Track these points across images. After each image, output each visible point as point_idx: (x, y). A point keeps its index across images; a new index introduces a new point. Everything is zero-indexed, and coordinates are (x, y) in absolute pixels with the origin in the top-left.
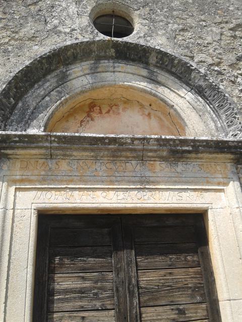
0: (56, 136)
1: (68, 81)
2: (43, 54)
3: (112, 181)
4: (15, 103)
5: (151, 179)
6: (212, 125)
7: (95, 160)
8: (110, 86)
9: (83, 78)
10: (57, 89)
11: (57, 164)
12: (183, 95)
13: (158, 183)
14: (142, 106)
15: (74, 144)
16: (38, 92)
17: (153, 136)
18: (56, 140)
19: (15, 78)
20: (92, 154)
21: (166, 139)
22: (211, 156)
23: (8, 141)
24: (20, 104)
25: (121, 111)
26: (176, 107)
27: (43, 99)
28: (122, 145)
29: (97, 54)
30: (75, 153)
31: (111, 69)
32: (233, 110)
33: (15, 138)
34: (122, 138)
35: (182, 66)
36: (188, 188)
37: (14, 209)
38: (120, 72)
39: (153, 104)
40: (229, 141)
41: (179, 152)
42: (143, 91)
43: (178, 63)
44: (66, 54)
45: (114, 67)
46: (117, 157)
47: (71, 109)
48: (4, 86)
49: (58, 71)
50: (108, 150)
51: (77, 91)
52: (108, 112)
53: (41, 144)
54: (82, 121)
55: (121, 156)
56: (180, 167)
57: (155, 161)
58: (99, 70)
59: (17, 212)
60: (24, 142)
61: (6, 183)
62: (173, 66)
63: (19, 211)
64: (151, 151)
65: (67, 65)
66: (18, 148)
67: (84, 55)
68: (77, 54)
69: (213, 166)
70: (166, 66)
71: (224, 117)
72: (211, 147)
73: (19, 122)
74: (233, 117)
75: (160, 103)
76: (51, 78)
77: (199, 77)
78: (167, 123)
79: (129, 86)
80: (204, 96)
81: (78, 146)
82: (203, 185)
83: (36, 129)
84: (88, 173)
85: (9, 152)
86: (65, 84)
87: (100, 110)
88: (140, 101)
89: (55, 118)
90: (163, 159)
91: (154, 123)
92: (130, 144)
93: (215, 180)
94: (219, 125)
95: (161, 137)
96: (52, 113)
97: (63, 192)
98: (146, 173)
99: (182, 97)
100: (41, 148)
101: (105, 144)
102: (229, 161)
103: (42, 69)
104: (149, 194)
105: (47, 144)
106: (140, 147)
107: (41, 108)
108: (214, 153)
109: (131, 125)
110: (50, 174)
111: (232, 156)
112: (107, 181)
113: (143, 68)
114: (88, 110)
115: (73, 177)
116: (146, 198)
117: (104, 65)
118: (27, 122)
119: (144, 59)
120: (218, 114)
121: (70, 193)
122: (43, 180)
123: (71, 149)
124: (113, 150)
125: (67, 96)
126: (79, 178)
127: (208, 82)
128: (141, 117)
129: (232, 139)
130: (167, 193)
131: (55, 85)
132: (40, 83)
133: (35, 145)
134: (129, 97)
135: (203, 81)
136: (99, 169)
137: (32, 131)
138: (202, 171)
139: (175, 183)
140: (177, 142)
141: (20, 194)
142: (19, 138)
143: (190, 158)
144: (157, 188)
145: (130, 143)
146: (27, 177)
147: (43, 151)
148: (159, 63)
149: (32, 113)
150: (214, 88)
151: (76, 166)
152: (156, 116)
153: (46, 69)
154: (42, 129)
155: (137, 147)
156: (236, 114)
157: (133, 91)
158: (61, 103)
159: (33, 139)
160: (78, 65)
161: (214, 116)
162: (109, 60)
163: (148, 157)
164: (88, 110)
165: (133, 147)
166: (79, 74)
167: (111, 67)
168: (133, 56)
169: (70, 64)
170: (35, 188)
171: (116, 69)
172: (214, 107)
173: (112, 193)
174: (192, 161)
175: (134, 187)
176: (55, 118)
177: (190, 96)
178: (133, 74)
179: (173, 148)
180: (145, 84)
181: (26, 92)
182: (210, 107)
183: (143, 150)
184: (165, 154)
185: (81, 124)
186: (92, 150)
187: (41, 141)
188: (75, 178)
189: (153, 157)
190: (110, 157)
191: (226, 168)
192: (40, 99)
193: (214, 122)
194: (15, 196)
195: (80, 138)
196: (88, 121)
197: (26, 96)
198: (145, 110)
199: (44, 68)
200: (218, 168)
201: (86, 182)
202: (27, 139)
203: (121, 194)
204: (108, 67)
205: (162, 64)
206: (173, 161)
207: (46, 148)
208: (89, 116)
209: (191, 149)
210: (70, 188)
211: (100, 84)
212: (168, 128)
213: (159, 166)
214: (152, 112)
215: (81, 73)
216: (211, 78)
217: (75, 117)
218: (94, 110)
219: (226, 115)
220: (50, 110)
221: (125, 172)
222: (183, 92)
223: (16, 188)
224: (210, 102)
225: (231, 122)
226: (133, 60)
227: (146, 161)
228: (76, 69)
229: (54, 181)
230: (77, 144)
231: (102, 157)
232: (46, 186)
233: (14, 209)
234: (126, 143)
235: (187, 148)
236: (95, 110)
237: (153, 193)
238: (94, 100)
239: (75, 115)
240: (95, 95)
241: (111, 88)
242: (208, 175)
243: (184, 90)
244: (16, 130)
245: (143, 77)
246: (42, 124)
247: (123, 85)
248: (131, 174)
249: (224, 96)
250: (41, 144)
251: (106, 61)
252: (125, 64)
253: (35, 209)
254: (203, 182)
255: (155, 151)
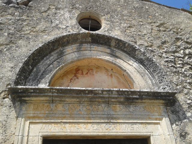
0: (56, 89)
1: (64, 56)
2: (50, 40)
3: (89, 117)
4: (32, 69)
5: (114, 116)
6: (150, 82)
7: (79, 104)
8: (88, 58)
9: (73, 54)
10: (57, 61)
11: (56, 107)
12: (131, 64)
13: (119, 119)
14: (107, 70)
15: (67, 94)
16: (46, 62)
17: (115, 89)
18: (56, 91)
19: (33, 54)
20: (78, 100)
21: (122, 91)
22: (150, 101)
23: (27, 92)
24: (35, 69)
25: (94, 73)
26: (127, 71)
27: (49, 66)
28: (96, 95)
29: (81, 41)
30: (67, 100)
31: (89, 49)
32: (162, 73)
33: (31, 90)
34: (96, 90)
35: (130, 47)
36: (137, 122)
37: (28, 136)
38: (94, 50)
39: (113, 69)
40: (161, 92)
41: (131, 99)
42: (107, 61)
43: (128, 46)
44: (63, 40)
45: (91, 48)
46: (93, 102)
47: (66, 71)
48: (26, 59)
49: (58, 50)
50: (87, 97)
51: (69, 61)
52: (87, 73)
53: (46, 94)
54: (71, 79)
55: (95, 101)
56: (132, 109)
57: (116, 104)
58: (82, 49)
59: (30, 138)
60: (36, 93)
61: (24, 119)
62: (125, 47)
63: (31, 137)
64: (114, 98)
65: (64, 46)
66: (33, 96)
67: (73, 41)
68: (70, 40)
69: (152, 108)
70: (121, 47)
71: (157, 77)
72: (150, 96)
73: (33, 80)
74: (162, 78)
75: (118, 69)
76: (54, 54)
77: (141, 54)
78: (122, 80)
79: (100, 58)
80: (144, 65)
81: (69, 95)
82: (146, 120)
83: (44, 85)
84: (75, 112)
85: (27, 99)
86: (62, 57)
87: (82, 72)
88: (106, 67)
89: (55, 78)
90: (121, 103)
91: (114, 80)
92: (101, 94)
93: (154, 117)
94: (154, 82)
95: (120, 89)
96: (54, 75)
97: (59, 125)
98: (111, 112)
99: (131, 65)
100: (46, 96)
101: (86, 94)
102: (162, 104)
103: (49, 49)
104: (113, 126)
105: (51, 94)
106: (107, 96)
107: (48, 72)
108: (152, 99)
109: (101, 82)
110: (51, 113)
111: (163, 102)
112: (87, 118)
113: (108, 48)
114: (75, 72)
115: (65, 115)
116: (111, 128)
117: (85, 46)
118: (38, 80)
119: (108, 43)
120: (153, 75)
121: (63, 125)
122: (47, 117)
123: (65, 97)
124: (90, 98)
125: (63, 65)
126: (69, 115)
127: (146, 56)
128: (106, 77)
129: (162, 91)
130: (124, 126)
131: (56, 58)
132: (48, 57)
133: (43, 94)
134: (99, 65)
135: (143, 56)
136: (81, 109)
137: (43, 85)
138: (145, 111)
139: (129, 118)
140: (130, 93)
141: (32, 126)
142: (34, 91)
143: (138, 103)
144: (118, 122)
145: (100, 93)
146: (37, 115)
147: (47, 98)
148: (117, 46)
149: (42, 74)
150: (150, 60)
151: (67, 108)
152: (115, 76)
153: (51, 49)
154: (48, 84)
155: (105, 96)
156: (164, 75)
157: (102, 61)
158: (60, 68)
159: (42, 91)
160: (70, 47)
161: (151, 76)
162: (87, 44)
163: (112, 102)
164: (75, 72)
165: (103, 96)
166: (70, 52)
167: (89, 48)
168: (101, 41)
169: (65, 46)
170: (42, 122)
171: (92, 49)
172: (150, 71)
173: (89, 125)
174: (139, 104)
175: (103, 121)
176: (55, 78)
177: (136, 65)
178: (102, 52)
179: (127, 96)
180: (109, 57)
181: (39, 62)
182: (148, 71)
183: (109, 98)
184: (122, 100)
185: (70, 81)
186: (78, 98)
187: (47, 92)
188: (67, 115)
189: (115, 102)
190: (89, 102)
191: (160, 108)
192: (47, 66)
193: (151, 80)
194: (29, 127)
195: (70, 90)
196: (75, 79)
197: (39, 65)
198: (109, 73)
199: (50, 49)
200: (155, 109)
201: (73, 118)
202: (38, 91)
203: (96, 126)
204: (87, 47)
205: (118, 46)
206: (127, 104)
207: (50, 96)
208: (75, 76)
209: (138, 97)
210: (63, 122)
211: (82, 57)
212: (123, 83)
213: (118, 107)
214: (113, 74)
215: (72, 51)
216: (148, 54)
217: (67, 76)
218: (78, 73)
219: (158, 76)
220: (53, 73)
221: (98, 111)
222: (131, 62)
223: (30, 122)
224: (148, 68)
225: (161, 80)
226: (102, 44)
227: (111, 104)
228: (69, 49)
229: (53, 118)
230: (69, 94)
231: (84, 102)
232: (49, 121)
233: (28, 136)
234: (98, 93)
235: (135, 96)
236: (79, 73)
237: (116, 125)
238: (79, 66)
239: (68, 75)
240: (79, 64)
241: (89, 60)
242: (150, 114)
243: (132, 61)
244: (32, 85)
245: (108, 53)
246: (48, 81)
247: (95, 58)
248: (102, 113)
249: (156, 65)
250: (46, 94)
251: (86, 44)
252: (97, 46)
253: (41, 136)
254: (146, 118)
255: (116, 98)
